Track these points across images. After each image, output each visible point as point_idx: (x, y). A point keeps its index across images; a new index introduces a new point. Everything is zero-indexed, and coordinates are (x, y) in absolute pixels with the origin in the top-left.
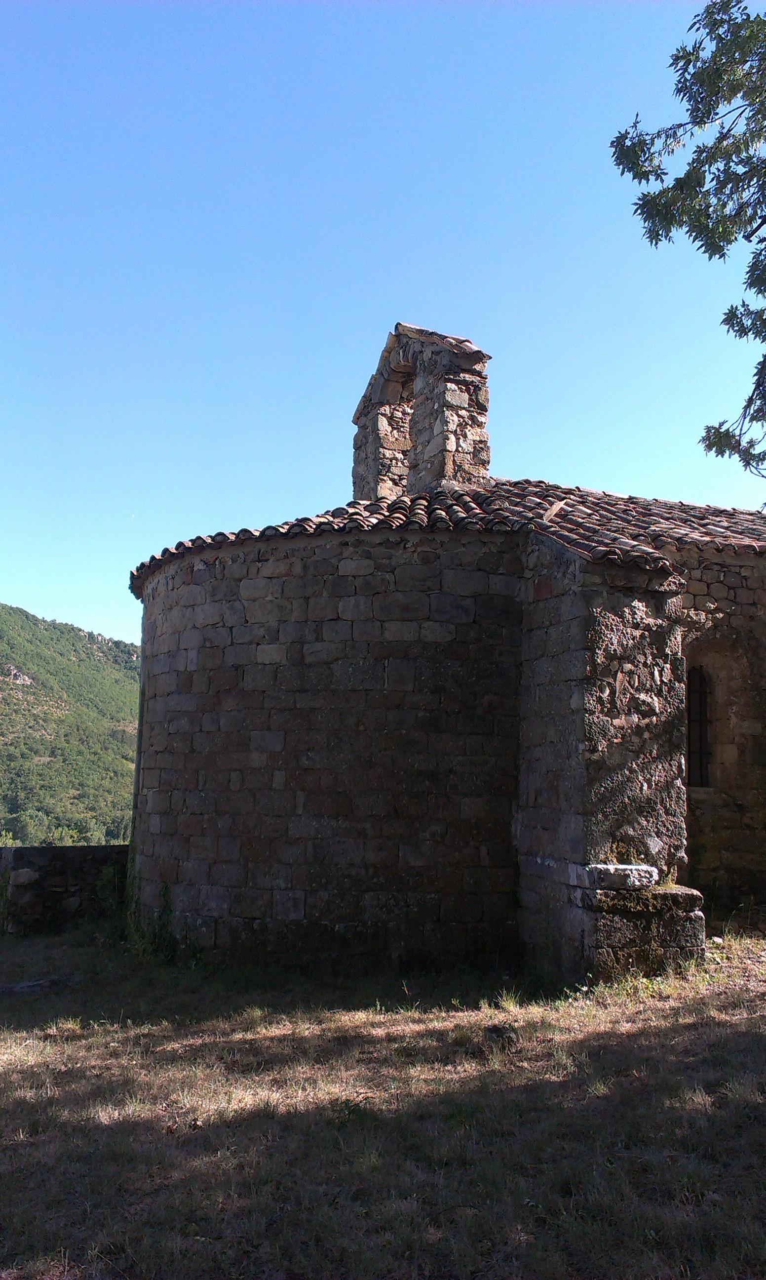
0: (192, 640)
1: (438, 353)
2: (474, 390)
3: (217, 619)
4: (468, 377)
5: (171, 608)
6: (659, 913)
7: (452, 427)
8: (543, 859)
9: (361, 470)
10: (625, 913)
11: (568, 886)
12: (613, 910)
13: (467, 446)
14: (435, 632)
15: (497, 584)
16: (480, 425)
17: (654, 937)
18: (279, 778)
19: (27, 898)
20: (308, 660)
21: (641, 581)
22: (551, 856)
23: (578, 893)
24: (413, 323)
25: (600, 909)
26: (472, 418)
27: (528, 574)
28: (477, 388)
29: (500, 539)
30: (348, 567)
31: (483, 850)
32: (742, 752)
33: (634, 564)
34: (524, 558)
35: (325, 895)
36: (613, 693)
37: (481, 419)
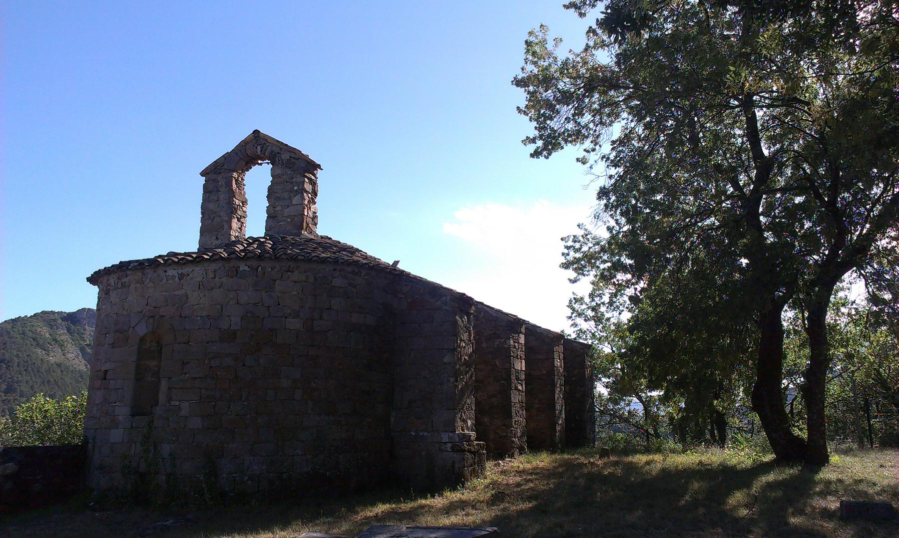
2: (314, 183)
4: (313, 178)
5: (212, 289)
9: (211, 206)
13: (311, 215)
23: (449, 445)
25: (464, 450)
30: (338, 282)
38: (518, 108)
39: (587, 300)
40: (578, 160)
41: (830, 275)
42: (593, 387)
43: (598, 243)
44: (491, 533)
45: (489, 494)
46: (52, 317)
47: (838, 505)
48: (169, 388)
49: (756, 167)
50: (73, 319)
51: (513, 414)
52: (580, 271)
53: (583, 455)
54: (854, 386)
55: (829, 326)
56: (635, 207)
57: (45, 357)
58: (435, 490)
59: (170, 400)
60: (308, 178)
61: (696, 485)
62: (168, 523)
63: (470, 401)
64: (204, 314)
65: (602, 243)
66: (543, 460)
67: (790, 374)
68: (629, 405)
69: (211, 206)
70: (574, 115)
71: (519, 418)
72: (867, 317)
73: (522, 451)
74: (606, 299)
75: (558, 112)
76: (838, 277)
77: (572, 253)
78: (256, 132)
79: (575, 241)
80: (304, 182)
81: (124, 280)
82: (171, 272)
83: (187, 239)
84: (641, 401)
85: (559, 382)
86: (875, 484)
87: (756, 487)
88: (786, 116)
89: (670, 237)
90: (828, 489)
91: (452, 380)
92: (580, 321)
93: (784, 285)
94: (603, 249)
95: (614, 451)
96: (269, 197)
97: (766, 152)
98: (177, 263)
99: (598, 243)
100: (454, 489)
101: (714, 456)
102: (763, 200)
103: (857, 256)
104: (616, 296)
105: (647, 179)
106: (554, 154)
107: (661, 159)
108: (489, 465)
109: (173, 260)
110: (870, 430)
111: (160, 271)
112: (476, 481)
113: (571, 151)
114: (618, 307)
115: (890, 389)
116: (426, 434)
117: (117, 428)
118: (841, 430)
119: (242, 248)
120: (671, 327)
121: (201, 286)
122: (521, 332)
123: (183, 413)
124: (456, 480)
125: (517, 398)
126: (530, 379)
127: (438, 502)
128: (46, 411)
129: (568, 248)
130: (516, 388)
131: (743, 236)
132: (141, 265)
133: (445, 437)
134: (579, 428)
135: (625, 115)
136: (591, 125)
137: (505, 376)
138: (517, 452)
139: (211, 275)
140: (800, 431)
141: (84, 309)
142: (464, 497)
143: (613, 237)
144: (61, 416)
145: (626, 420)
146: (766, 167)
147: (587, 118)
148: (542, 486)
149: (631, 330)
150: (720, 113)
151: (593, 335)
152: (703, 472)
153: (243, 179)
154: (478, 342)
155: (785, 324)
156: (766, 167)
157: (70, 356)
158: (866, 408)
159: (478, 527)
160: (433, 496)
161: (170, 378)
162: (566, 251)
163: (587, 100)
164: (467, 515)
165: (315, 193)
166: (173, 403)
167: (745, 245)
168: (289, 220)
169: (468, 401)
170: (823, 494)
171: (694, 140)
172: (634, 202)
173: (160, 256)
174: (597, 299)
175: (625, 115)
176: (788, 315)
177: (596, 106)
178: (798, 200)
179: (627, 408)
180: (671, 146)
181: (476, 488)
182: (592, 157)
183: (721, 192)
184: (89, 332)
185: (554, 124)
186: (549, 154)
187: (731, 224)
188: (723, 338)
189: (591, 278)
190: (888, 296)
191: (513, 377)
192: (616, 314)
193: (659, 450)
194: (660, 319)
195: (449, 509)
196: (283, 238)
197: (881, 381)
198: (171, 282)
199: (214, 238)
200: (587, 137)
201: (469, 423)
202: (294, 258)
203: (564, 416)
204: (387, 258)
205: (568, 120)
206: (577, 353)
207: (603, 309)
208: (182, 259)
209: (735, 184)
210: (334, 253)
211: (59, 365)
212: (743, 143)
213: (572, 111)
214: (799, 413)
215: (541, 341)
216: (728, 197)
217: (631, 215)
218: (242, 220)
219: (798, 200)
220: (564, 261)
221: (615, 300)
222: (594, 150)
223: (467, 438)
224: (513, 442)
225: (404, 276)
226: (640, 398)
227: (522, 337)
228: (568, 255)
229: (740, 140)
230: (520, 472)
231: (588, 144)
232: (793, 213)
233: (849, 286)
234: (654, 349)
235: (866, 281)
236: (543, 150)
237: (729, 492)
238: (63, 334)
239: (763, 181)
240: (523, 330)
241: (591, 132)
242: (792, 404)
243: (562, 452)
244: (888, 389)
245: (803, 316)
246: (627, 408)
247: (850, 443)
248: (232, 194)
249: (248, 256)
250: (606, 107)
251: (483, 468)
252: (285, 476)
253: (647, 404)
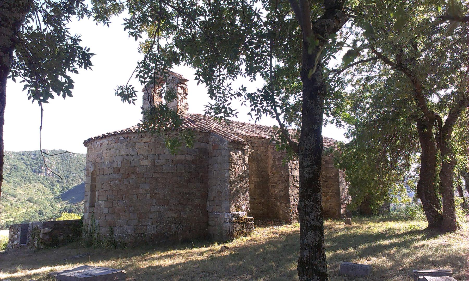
0: (120, 159)
1: (175, 78)
2: (185, 89)
3: (128, 153)
4: (183, 86)
6: (246, 223)
7: (180, 99)
8: (216, 213)
10: (239, 223)
11: (225, 218)
12: (237, 222)
13: (183, 104)
14: (189, 157)
15: (203, 145)
16: (186, 99)
17: (245, 227)
18: (148, 196)
19: (47, 237)
20: (156, 165)
21: (240, 146)
22: (219, 212)
23: (228, 219)
25: (234, 222)
26: (184, 97)
27: (210, 143)
28: (185, 89)
29: (204, 134)
31: (200, 212)
32: (255, 186)
33: (239, 143)
34: (209, 139)
35: (162, 226)
36: (235, 173)
37: (186, 97)
82: (98, 143)
91: (229, 185)
116: (219, 214)
139: (110, 143)
159: (167, 268)
252: (142, 235)
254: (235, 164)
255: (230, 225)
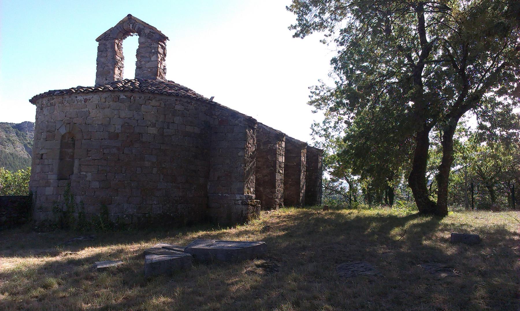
1: (153, 33)
2: (164, 48)
4: (164, 45)
5: (104, 108)
9: (103, 60)
13: (162, 67)
18: (155, 170)
20: (165, 134)
23: (240, 201)
24: (134, 15)
25: (249, 204)
29: (209, 106)
30: (178, 107)
35: (168, 206)
38: (287, 7)
39: (322, 125)
40: (321, 41)
41: (458, 111)
42: (322, 174)
43: (329, 91)
44: (261, 245)
45: (261, 228)
46: (6, 126)
47: (450, 236)
48: (80, 165)
49: (422, 49)
50: (19, 128)
51: (277, 186)
52: (318, 106)
53: (314, 209)
54: (466, 176)
55: (454, 140)
56: (351, 69)
57: (4, 149)
58: (231, 225)
59: (80, 171)
60: (161, 45)
61: (374, 224)
62: (80, 239)
63: (252, 177)
64: (100, 123)
65: (332, 91)
66: (292, 211)
67: (432, 168)
68: (341, 184)
69: (103, 60)
70: (319, 13)
71: (280, 188)
72: (476, 136)
73: (280, 206)
74: (332, 125)
75: (310, 11)
76: (461, 113)
77: (314, 96)
78: (129, 16)
79: (316, 89)
80: (158, 47)
81: (51, 102)
82: (79, 98)
83: (89, 80)
84: (348, 182)
85: (303, 169)
86: (471, 226)
87: (407, 226)
88: (441, 18)
89: (370, 87)
90: (446, 228)
91: (243, 165)
92: (317, 137)
93: (432, 116)
94: (332, 95)
95: (331, 208)
96: (137, 56)
97: (428, 40)
98: (83, 92)
99: (329, 91)
100: (242, 225)
101: (385, 211)
102: (424, 69)
103: (474, 102)
104: (338, 123)
105: (359, 52)
106: (306, 37)
107: (368, 42)
108: (262, 213)
109: (80, 91)
110: (472, 200)
111: (73, 96)
112: (254, 221)
113: (316, 35)
114: (339, 129)
115: (486, 178)
116: (227, 195)
117: (49, 186)
118: (457, 200)
119: (121, 85)
120: (367, 139)
121: (97, 106)
122: (283, 141)
123: (87, 179)
124: (243, 220)
125: (279, 177)
126: (287, 167)
127: (233, 231)
128: (7, 178)
129: (311, 92)
130: (279, 172)
131: (411, 88)
132: (62, 93)
133: (238, 197)
134: (313, 194)
135: (349, 15)
136: (329, 20)
137: (273, 165)
138: (278, 207)
139: (103, 100)
140: (434, 198)
141: (26, 122)
142: (247, 229)
143: (338, 88)
144: (15, 181)
145: (339, 193)
146: (428, 48)
147: (327, 15)
148: (290, 224)
149: (345, 140)
150: (403, 15)
151: (324, 145)
152: (379, 218)
153: (121, 44)
154: (258, 145)
155: (430, 139)
156: (428, 48)
157: (18, 149)
158: (472, 190)
160: (230, 228)
161: (80, 159)
162: (311, 95)
163: (327, 4)
164: (249, 237)
165: (165, 55)
166: (82, 173)
167: (412, 93)
168: (149, 70)
169: (252, 177)
170: (442, 231)
171: (388, 31)
172: (351, 66)
173: (72, 88)
174: (327, 125)
175: (349, 15)
176: (432, 134)
177: (333, 9)
178: (444, 68)
179: (340, 186)
180: (375, 33)
181: (255, 224)
182: (328, 39)
183: (401, 62)
184: (30, 136)
185: (309, 17)
186: (304, 36)
187: (405, 82)
188: (396, 146)
189: (324, 111)
190: (488, 125)
191: (277, 166)
192: (337, 133)
193: (356, 208)
194: (361, 135)
195: (238, 235)
196: (146, 80)
197: (481, 174)
198: (79, 103)
199: (104, 79)
200: (327, 27)
201: (252, 190)
202: (152, 92)
203: (305, 188)
204: (207, 96)
205: (315, 16)
206: (315, 155)
207: (330, 130)
208: (86, 90)
209: (409, 57)
210: (176, 90)
211: (12, 154)
212: (416, 34)
213: (319, 11)
214: (435, 190)
215: (294, 147)
216: (405, 65)
217: (349, 74)
218: (121, 69)
219: (444, 68)
220: (310, 101)
221: (337, 125)
222: (330, 35)
223: (250, 198)
224: (276, 201)
225: (216, 105)
226: (347, 180)
227: (284, 143)
228: (312, 97)
229: (414, 32)
230: (279, 217)
231: (327, 31)
232: (439, 75)
233: (468, 119)
234: (358, 153)
235: (477, 115)
236: (301, 33)
237: (392, 228)
238: (13, 136)
239: (425, 58)
240: (284, 139)
241: (329, 24)
242: (431, 185)
243: (303, 208)
244: (484, 178)
245: (441, 134)
246: (340, 186)
247: (461, 207)
248: (115, 53)
249: (124, 90)
250: (338, 9)
251: (259, 214)
253: (350, 183)
254: (249, 143)
255: (244, 207)
